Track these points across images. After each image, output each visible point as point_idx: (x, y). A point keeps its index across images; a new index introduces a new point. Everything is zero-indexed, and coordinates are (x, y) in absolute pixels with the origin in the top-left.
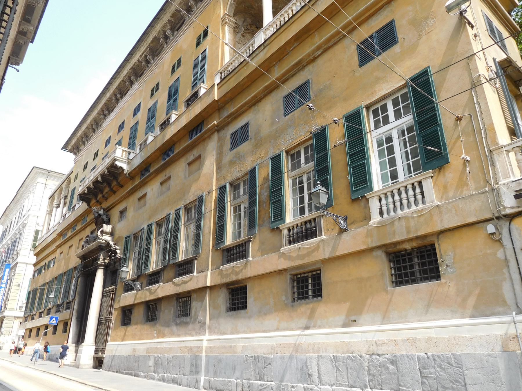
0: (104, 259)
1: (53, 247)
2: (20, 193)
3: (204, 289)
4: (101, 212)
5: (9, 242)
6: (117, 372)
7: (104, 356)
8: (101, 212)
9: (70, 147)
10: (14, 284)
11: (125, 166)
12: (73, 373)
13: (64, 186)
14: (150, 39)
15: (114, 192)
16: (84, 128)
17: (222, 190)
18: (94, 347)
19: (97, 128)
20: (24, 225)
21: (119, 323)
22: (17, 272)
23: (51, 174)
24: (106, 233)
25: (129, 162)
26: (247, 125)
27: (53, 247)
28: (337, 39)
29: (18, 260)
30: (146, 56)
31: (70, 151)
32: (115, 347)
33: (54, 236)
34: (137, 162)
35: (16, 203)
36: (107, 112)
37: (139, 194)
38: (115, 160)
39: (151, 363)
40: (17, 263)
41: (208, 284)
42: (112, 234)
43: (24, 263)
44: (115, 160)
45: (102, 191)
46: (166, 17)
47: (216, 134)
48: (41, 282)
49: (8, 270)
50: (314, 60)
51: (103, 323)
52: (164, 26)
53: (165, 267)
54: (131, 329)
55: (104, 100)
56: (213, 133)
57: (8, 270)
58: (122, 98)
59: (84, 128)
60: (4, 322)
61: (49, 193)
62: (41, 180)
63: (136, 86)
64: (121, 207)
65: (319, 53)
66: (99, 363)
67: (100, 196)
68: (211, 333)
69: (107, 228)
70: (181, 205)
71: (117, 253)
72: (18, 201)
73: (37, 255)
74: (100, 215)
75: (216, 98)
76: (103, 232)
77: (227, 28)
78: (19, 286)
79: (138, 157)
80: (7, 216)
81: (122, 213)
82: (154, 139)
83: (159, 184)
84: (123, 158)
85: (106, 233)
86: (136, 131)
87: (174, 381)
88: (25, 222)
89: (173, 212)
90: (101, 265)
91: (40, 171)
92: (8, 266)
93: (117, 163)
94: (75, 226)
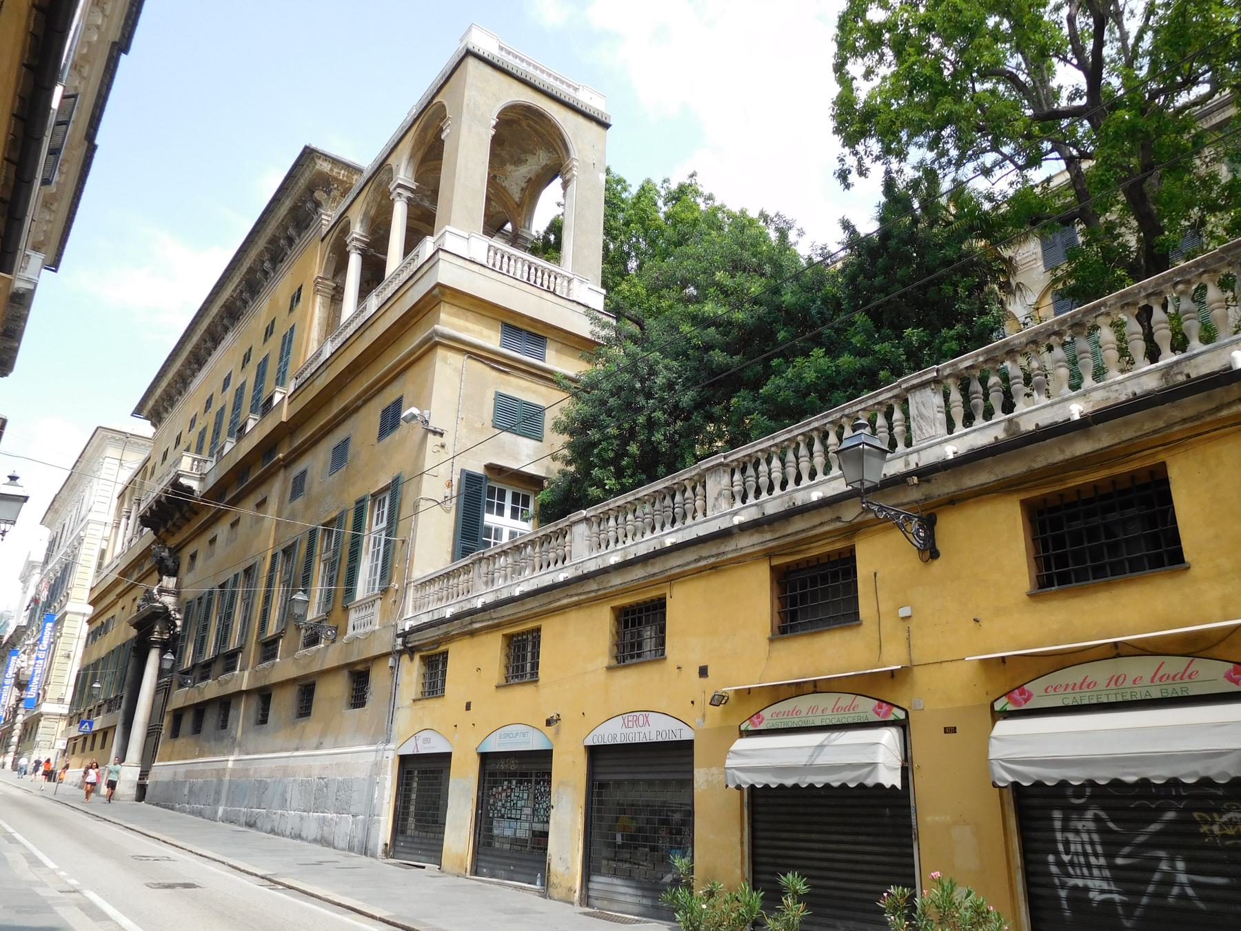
0: (161, 633)
1: (112, 597)
2: (78, 470)
3: (241, 693)
4: (165, 554)
5: (57, 567)
6: (157, 805)
7: (148, 782)
8: (165, 554)
9: (145, 412)
10: (58, 653)
11: (195, 485)
12: (107, 811)
13: (138, 479)
14: (244, 269)
15: (188, 520)
16: (164, 384)
17: (274, 556)
18: (139, 769)
19: (274, 269)
20: (80, 540)
21: (169, 735)
22: (64, 631)
23: (133, 440)
24: (168, 592)
25: (202, 479)
26: (304, 473)
27: (112, 597)
28: (314, 442)
29: (68, 608)
30: (241, 292)
31: (146, 418)
32: (162, 770)
33: (114, 576)
34: (211, 481)
35: (72, 490)
37: (208, 536)
38: (179, 476)
39: (186, 791)
40: (66, 613)
41: (244, 688)
42: (177, 593)
43: (78, 614)
44: (179, 476)
45: (172, 517)
46: (261, 243)
47: (282, 471)
48: (95, 656)
49: (50, 625)
50: (357, 409)
51: (152, 732)
52: (261, 254)
53: (216, 657)
54: (180, 742)
55: (189, 347)
56: (279, 470)
57: (50, 625)
58: (215, 349)
59: (164, 384)
60: (42, 724)
61: (119, 488)
62: (112, 452)
63: (229, 337)
64: (190, 549)
65: (360, 402)
66: (142, 792)
67: (170, 523)
68: (241, 753)
69: (169, 582)
70: (240, 570)
71: (176, 626)
72: (75, 485)
73: (93, 603)
74: (162, 559)
75: (284, 419)
76: (161, 591)
77: (319, 299)
78: (68, 657)
79: (214, 470)
80: (56, 512)
81: (193, 557)
82: (257, 428)
83: (228, 526)
84: (193, 470)
85: (168, 592)
86: (242, 393)
87: (200, 814)
88: (82, 534)
89: (231, 576)
90: (155, 642)
91: (110, 435)
92: (50, 618)
93: (182, 480)
94: (142, 565)
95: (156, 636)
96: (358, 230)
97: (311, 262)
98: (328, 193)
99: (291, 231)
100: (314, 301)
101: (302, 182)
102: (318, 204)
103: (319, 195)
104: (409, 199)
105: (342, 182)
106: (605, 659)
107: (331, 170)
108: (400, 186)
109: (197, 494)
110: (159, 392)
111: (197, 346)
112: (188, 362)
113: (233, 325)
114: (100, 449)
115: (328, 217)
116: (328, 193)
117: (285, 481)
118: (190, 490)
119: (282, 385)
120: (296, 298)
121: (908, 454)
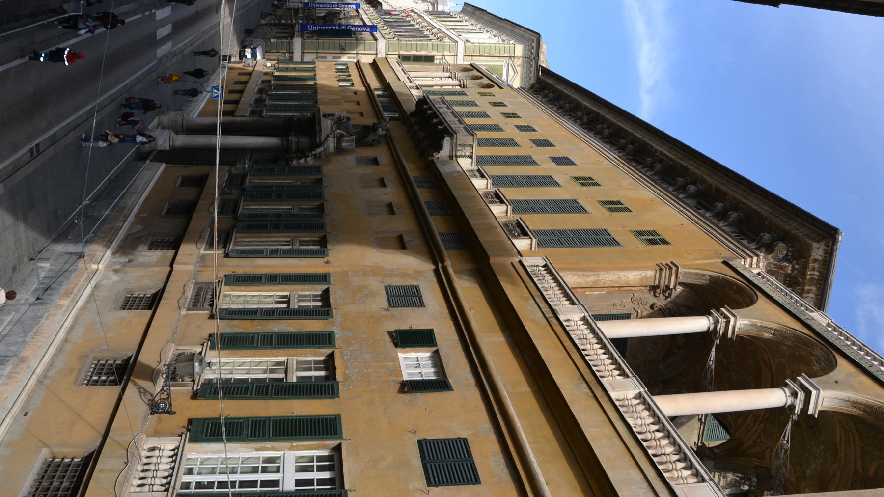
16: (567, 91)
19: (689, 197)
30: (661, 161)
36: (586, 120)
46: (713, 181)
52: (703, 181)
80: (474, 14)
95: (293, 139)
96: (741, 322)
97: (700, 249)
98: (786, 259)
99: (733, 215)
100: (647, 268)
101: (791, 226)
102: (769, 249)
103: (781, 248)
104: (792, 407)
105: (804, 275)
106: (450, 393)
107: (815, 260)
108: (808, 394)
109: (436, 155)
110: (561, 88)
111: (604, 120)
112: (589, 112)
113: (628, 154)
114: (520, 39)
115: (755, 266)
116: (786, 259)
117: (418, 273)
118: (439, 148)
119: (539, 245)
120: (653, 239)
121: (685, 459)
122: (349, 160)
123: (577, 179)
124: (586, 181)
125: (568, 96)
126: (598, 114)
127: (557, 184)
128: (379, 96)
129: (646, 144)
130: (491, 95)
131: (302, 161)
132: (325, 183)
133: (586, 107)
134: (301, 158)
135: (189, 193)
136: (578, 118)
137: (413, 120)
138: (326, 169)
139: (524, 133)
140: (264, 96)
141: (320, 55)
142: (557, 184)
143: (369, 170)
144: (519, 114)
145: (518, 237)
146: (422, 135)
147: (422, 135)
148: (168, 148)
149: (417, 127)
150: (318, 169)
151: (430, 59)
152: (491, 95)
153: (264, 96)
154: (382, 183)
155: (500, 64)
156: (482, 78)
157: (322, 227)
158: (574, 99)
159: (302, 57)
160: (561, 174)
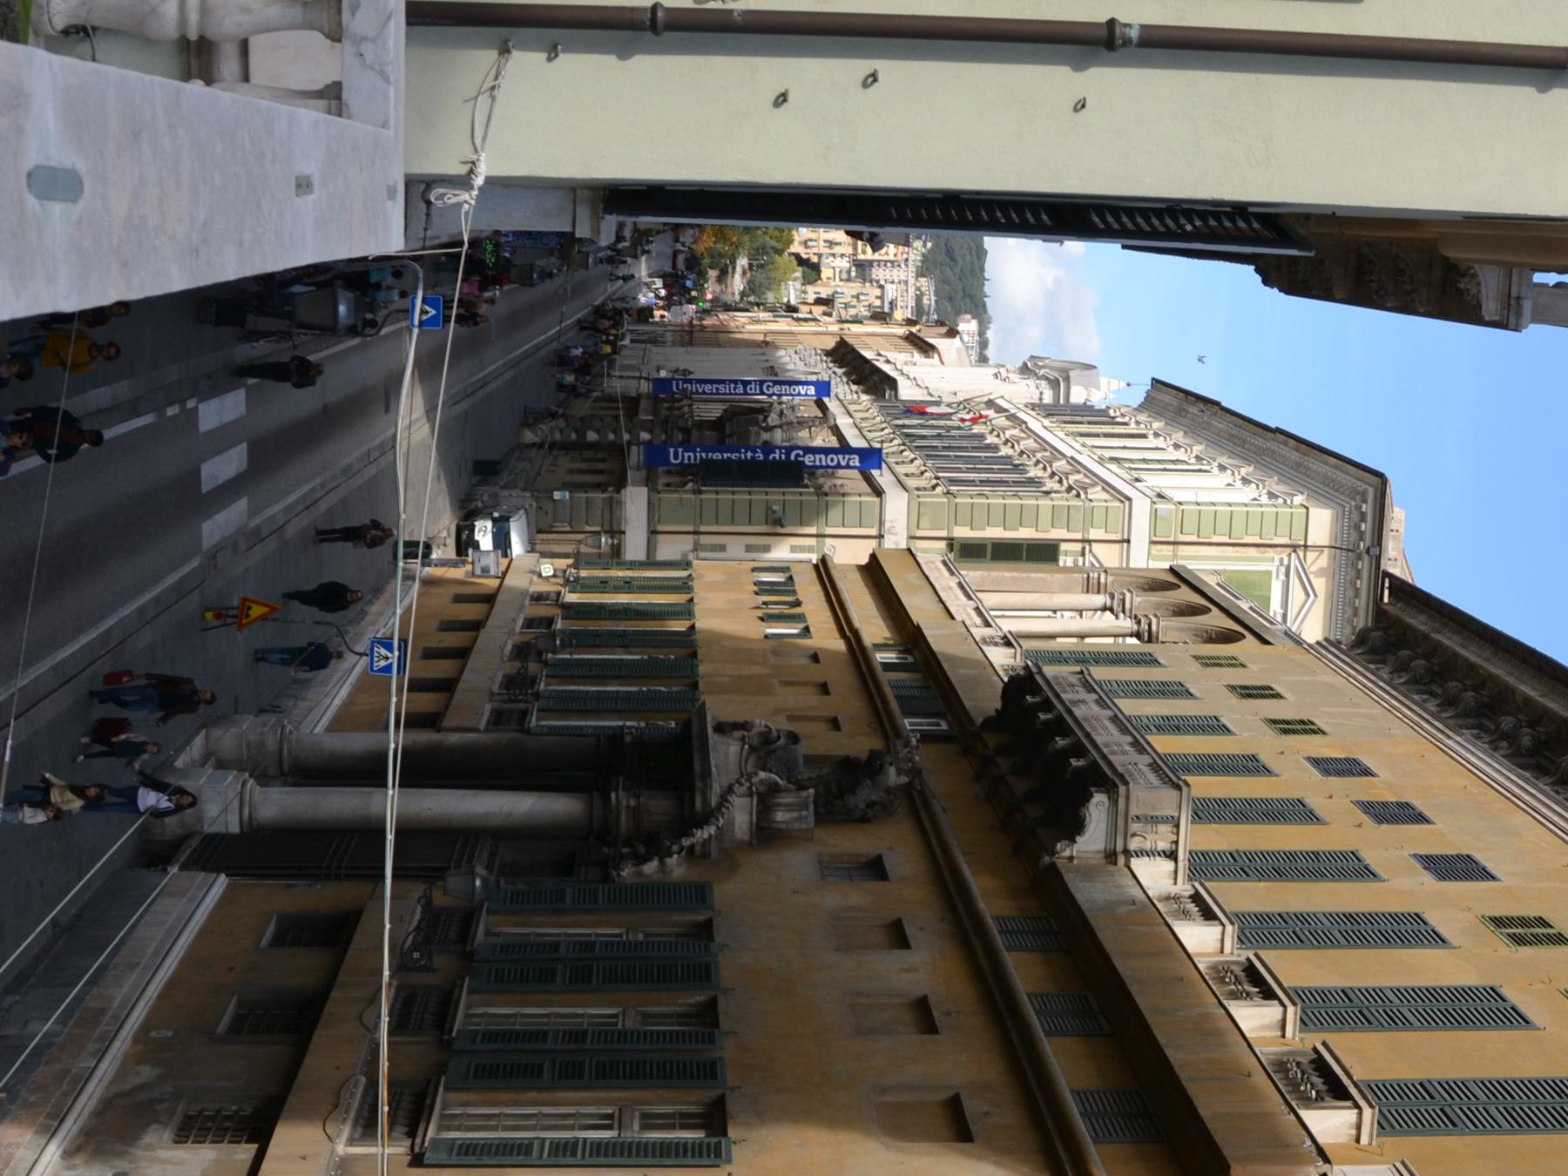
16: (1499, 670)
36: (1526, 741)
122: (797, 863)
123: (1499, 922)
124: (1456, 868)
125: (1472, 667)
126: (1456, 655)
127: (1437, 939)
128: (888, 667)
129: (1506, 686)
130: (1233, 663)
131: (650, 868)
132: (721, 936)
133: (1528, 700)
134: (646, 859)
135: (301, 969)
136: (1504, 736)
137: (992, 740)
138: (723, 892)
139: (1335, 781)
140: (533, 667)
141: (704, 539)
142: (1437, 939)
143: (857, 896)
144: (1320, 723)
145: (1316, 1103)
146: (1020, 786)
147: (1020, 786)
148: (234, 828)
149: (1004, 763)
150: (699, 894)
151: (1044, 553)
152: (1233, 663)
153: (533, 667)
154: (898, 937)
155: (1262, 567)
156: (1206, 611)
157: (710, 1071)
158: (1492, 677)
159: (651, 547)
160: (1451, 907)
